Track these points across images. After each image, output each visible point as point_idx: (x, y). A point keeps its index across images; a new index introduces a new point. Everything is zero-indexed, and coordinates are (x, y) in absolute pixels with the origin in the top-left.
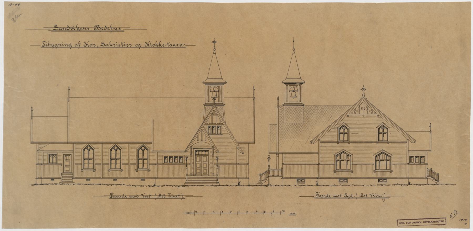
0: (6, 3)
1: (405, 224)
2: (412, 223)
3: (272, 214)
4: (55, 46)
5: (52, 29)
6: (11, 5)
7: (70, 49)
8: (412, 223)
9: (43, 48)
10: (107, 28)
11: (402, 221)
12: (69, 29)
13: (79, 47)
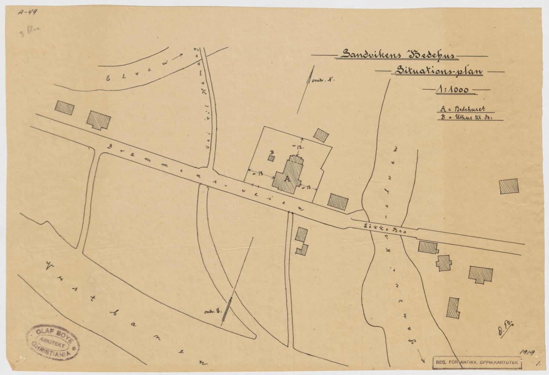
0: (9, 9)
6: (22, 13)
11: (442, 359)
12: (430, 56)
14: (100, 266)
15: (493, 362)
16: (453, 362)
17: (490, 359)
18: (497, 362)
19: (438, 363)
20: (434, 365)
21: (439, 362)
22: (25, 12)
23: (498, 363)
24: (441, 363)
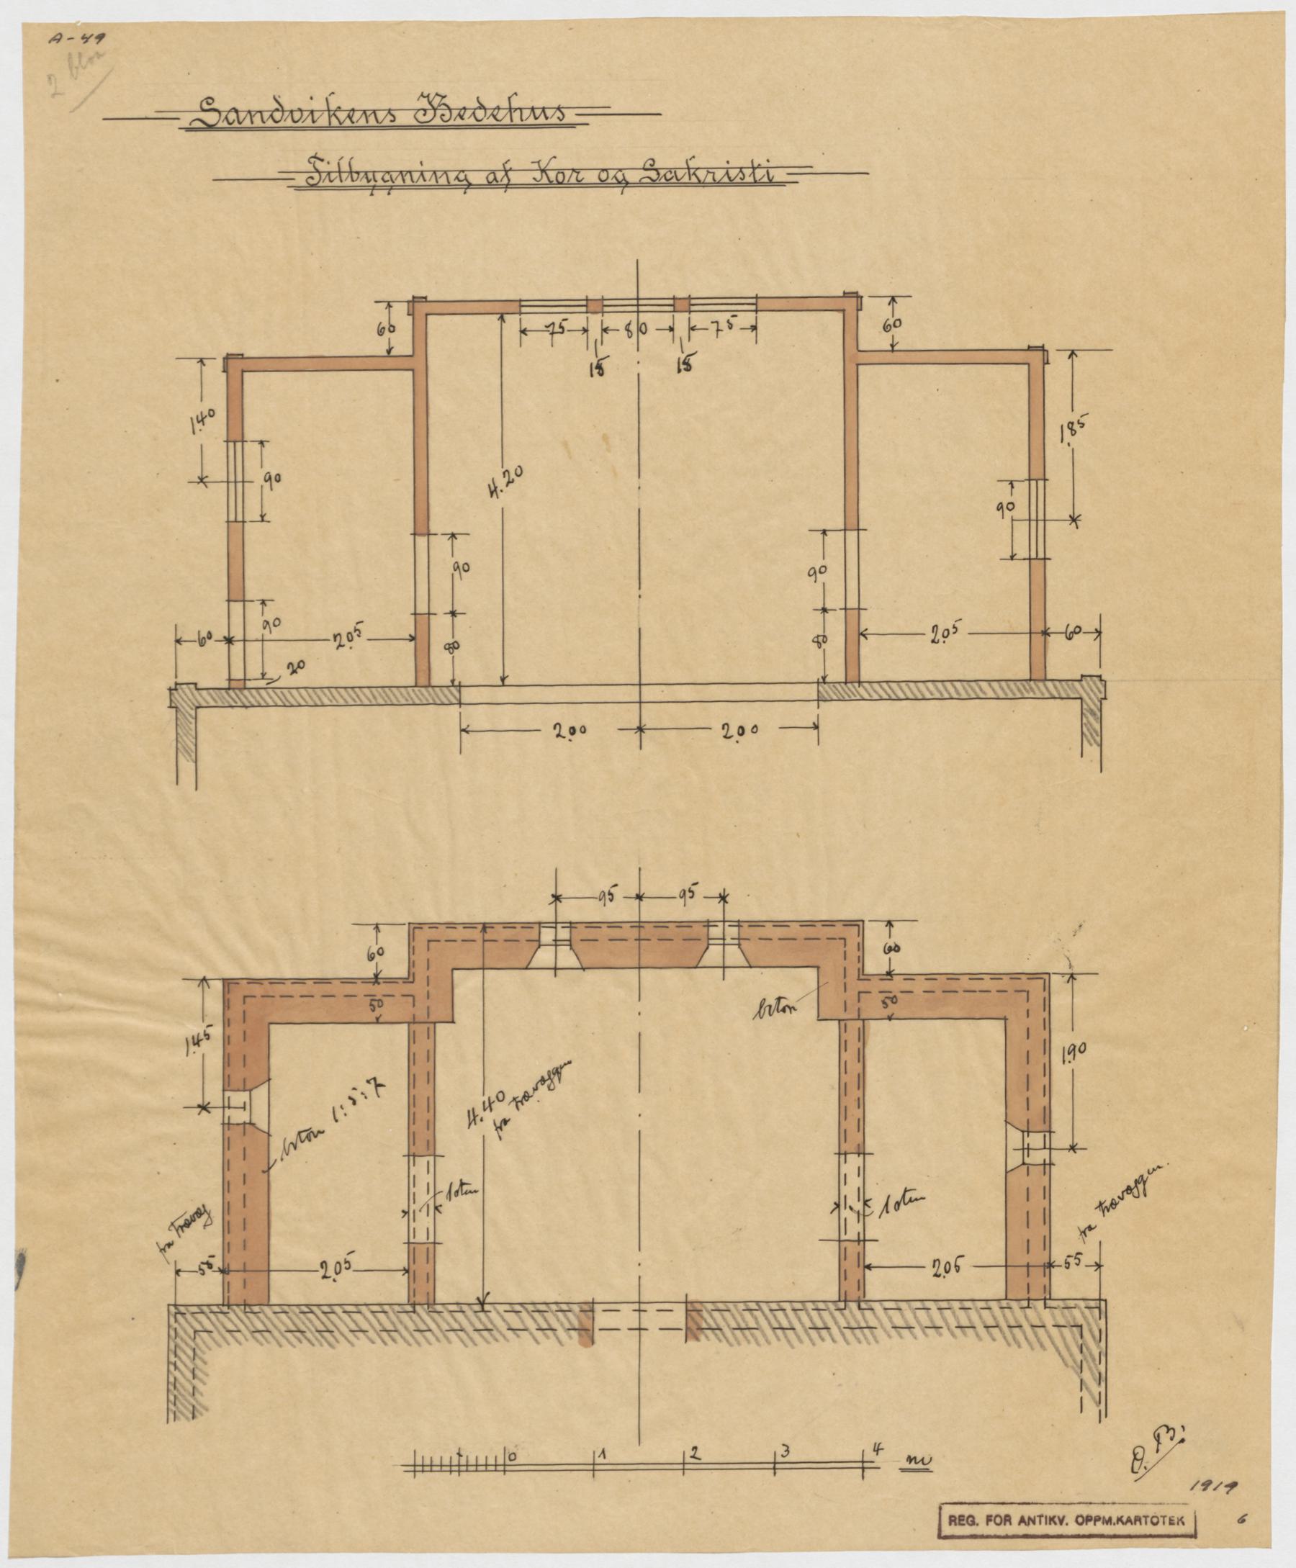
1: (982, 1529)
2: (1015, 1520)
3: (774, 1469)
4: (380, 183)
5: (186, 120)
6: (59, 40)
7: (372, 194)
8: (1015, 1520)
9: (311, 195)
10: (489, 112)
11: (965, 1511)
13: (507, 186)
14: (639, 399)
15: (1114, 1520)
16: (998, 1520)
17: (1105, 1512)
18: (1124, 1519)
19: (953, 1523)
20: (943, 1528)
21: (957, 1521)
22: (69, 39)
23: (1129, 1524)
24: (962, 1522)
